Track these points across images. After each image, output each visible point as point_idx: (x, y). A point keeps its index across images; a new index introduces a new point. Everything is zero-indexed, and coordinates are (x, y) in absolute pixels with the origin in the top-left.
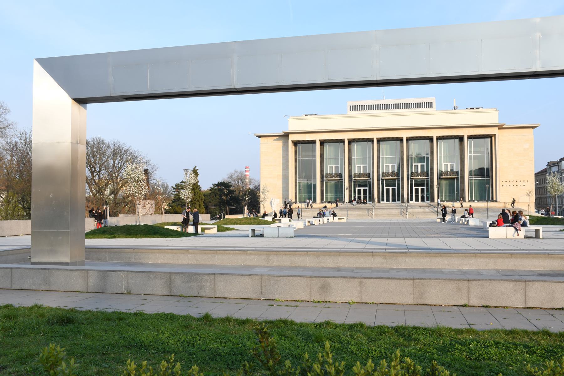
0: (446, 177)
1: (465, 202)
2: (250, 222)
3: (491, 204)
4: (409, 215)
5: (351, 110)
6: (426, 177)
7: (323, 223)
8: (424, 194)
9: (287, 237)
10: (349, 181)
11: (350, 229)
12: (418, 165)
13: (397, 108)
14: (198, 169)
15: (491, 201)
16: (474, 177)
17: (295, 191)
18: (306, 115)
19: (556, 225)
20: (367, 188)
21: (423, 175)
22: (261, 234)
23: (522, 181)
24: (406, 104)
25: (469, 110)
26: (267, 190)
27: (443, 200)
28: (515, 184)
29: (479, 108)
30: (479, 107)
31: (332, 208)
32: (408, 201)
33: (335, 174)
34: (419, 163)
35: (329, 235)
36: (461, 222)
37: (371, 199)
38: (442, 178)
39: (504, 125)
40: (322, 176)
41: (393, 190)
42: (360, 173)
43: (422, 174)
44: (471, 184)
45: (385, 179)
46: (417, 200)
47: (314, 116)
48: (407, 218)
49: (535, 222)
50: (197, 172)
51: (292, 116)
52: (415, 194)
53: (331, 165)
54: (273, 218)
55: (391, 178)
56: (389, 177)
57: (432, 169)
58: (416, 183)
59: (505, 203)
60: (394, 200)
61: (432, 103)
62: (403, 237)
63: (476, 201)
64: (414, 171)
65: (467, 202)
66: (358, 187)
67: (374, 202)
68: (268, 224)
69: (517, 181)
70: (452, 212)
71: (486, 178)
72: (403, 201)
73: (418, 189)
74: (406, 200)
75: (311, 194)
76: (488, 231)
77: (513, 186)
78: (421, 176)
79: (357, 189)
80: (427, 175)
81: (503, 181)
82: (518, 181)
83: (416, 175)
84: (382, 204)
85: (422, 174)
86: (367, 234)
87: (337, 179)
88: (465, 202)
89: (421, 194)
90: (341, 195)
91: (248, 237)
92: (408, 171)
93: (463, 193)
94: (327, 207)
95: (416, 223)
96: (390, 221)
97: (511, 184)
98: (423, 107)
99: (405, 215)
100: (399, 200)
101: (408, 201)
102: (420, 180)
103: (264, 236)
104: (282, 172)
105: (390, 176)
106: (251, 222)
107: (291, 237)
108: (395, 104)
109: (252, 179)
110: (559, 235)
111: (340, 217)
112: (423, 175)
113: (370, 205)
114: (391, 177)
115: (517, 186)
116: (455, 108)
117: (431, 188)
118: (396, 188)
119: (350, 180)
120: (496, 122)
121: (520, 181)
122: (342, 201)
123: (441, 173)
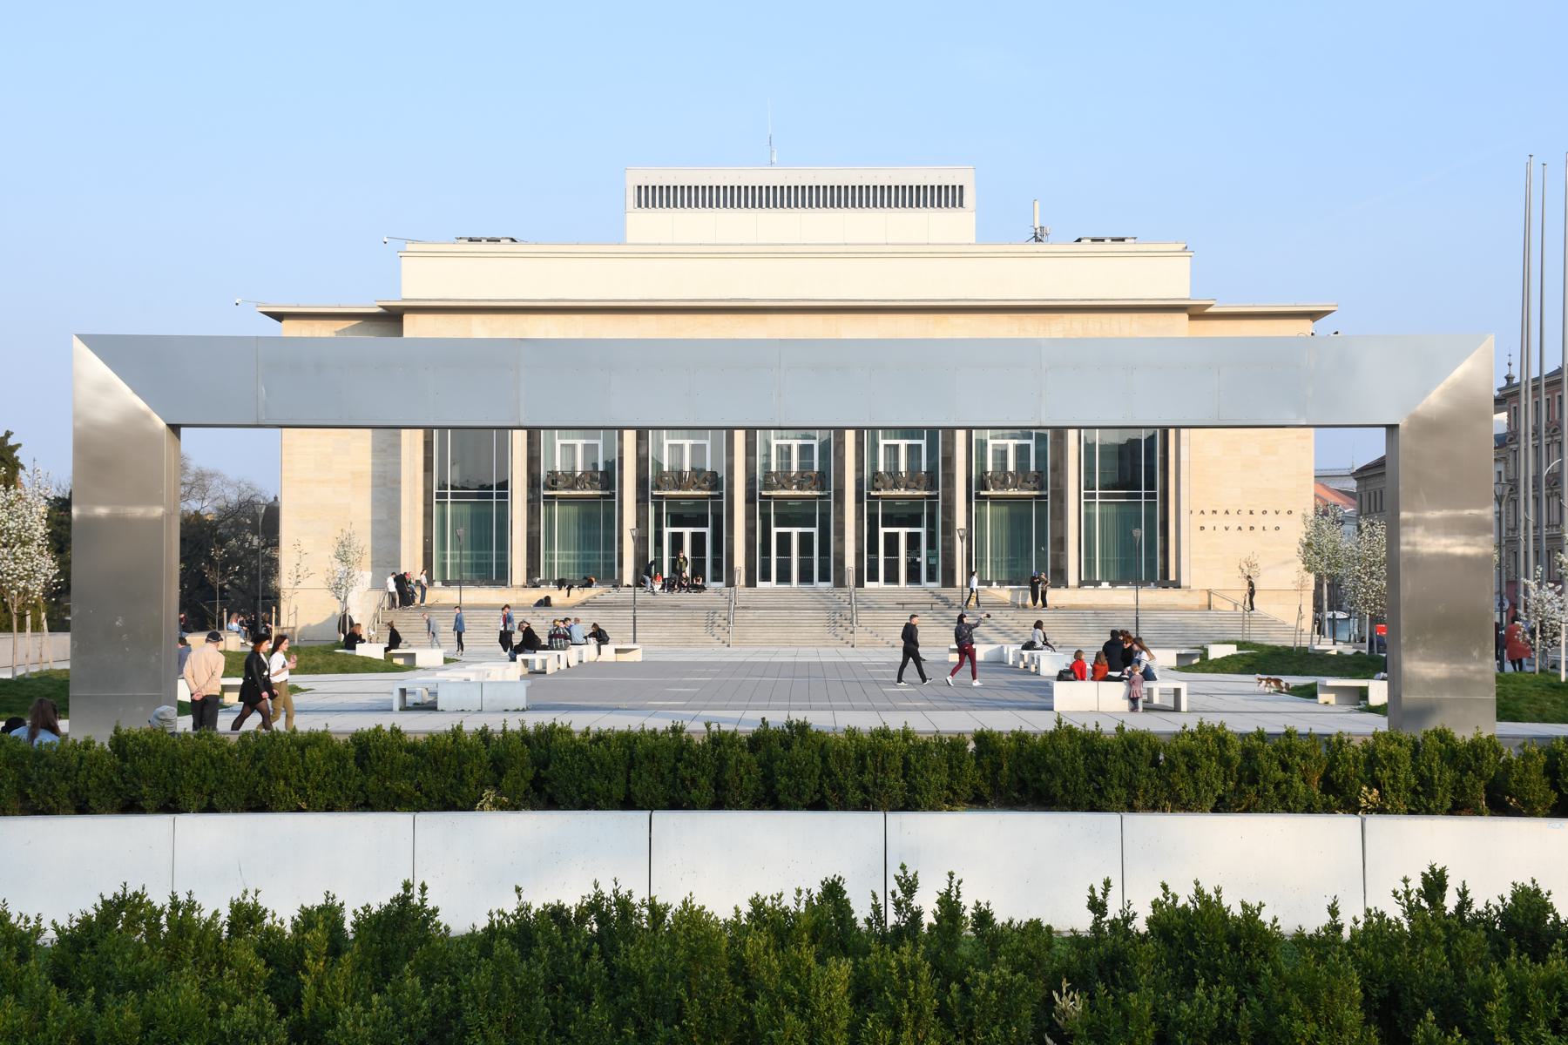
0: (999, 493)
1: (1067, 587)
2: (311, 664)
3: (1151, 596)
4: (860, 636)
5: (640, 206)
6: (926, 493)
7: (568, 666)
8: (919, 556)
9: (506, 710)
10: (638, 501)
11: (670, 687)
12: (897, 447)
13: (832, 206)
14: (19, 445)
15: (1158, 585)
16: (1102, 496)
17: (425, 538)
18: (471, 240)
19: (1307, 675)
20: (708, 531)
21: (914, 484)
22: (415, 704)
23: (1271, 513)
24: (861, 187)
25: (1087, 245)
26: (355, 545)
27: (989, 579)
28: (1247, 520)
29: (1123, 240)
30: (1122, 236)
31: (573, 607)
32: (859, 583)
33: (583, 473)
34: (902, 438)
35: (624, 704)
36: (1022, 665)
37: (723, 571)
38: (985, 497)
39: (1210, 306)
40: (533, 481)
41: (806, 540)
42: (680, 473)
43: (913, 478)
44: (1090, 518)
45: (776, 498)
46: (892, 577)
47: (505, 246)
48: (853, 646)
49: (1245, 665)
50: (15, 454)
51: (414, 241)
52: (885, 555)
53: (567, 438)
54: (386, 650)
55: (799, 493)
56: (790, 489)
57: (949, 461)
58: (888, 511)
59: (1209, 592)
60: (806, 577)
61: (961, 187)
62: (832, 708)
63: (1105, 585)
64: (881, 469)
65: (1073, 587)
66: (672, 526)
67: (731, 584)
68: (377, 672)
69: (1251, 513)
70: (504, 730)
71: (1143, 500)
72: (840, 583)
73: (897, 534)
74: (850, 578)
75: (488, 552)
76: (1051, 691)
77: (1240, 528)
78: (907, 488)
79: (667, 531)
80: (932, 484)
81: (1202, 512)
82: (1258, 512)
83: (888, 485)
84: (764, 591)
85: (912, 480)
86: (709, 701)
87: (591, 493)
88: (1067, 587)
89: (908, 554)
90: (606, 557)
91: (391, 710)
92: (859, 468)
93: (1061, 553)
94: (554, 601)
95: (878, 667)
96: (792, 659)
97: (1234, 522)
98: (925, 205)
99: (848, 637)
100: (824, 577)
101: (859, 583)
102: (906, 502)
103: (439, 707)
104: (370, 461)
105: (794, 487)
106: (314, 664)
107: (518, 710)
108: (818, 187)
109: (212, 476)
110: (1257, 704)
111: (622, 643)
112: (914, 484)
113: (717, 596)
114: (799, 489)
115: (1252, 528)
116: (1036, 234)
117: (942, 534)
118: (815, 531)
119: (640, 497)
120: (1180, 292)
121: (1265, 512)
122: (610, 576)
123: (982, 477)
